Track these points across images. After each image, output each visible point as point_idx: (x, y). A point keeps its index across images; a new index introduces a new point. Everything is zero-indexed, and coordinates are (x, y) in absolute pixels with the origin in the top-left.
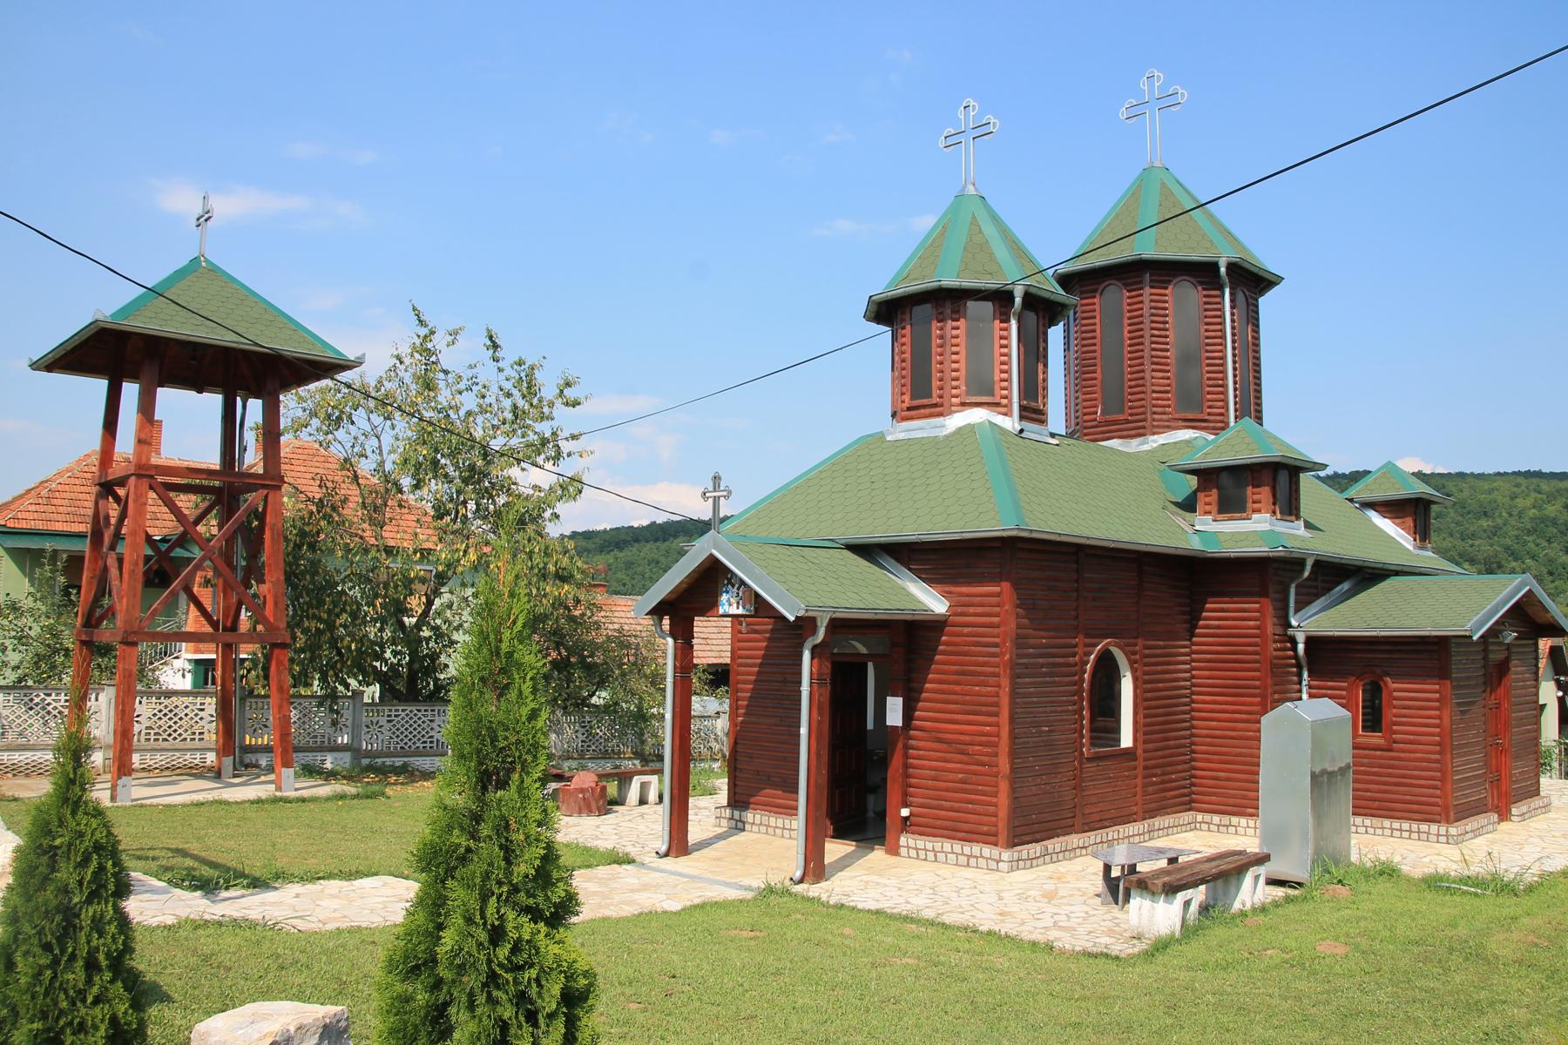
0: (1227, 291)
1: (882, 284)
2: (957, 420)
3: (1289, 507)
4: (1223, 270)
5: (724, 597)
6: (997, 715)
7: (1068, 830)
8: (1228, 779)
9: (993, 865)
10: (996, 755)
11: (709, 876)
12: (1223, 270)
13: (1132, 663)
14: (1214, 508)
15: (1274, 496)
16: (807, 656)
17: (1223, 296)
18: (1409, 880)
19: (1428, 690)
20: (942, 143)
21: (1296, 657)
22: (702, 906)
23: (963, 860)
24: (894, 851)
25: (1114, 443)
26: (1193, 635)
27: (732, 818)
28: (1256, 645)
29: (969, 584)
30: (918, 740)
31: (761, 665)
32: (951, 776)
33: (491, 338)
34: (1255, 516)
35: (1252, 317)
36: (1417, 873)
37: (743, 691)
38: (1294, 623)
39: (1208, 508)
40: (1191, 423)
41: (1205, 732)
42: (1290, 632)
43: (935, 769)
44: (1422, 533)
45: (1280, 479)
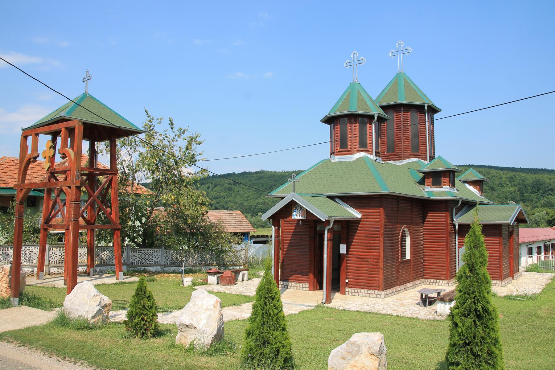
0: (427, 114)
3: (453, 184)
4: (426, 108)
5: (294, 213)
10: (379, 262)
12: (426, 108)
13: (410, 232)
16: (326, 232)
18: (500, 297)
21: (455, 230)
22: (303, 311)
24: (344, 293)
25: (391, 162)
26: (424, 224)
27: (283, 285)
29: (369, 209)
30: (351, 258)
31: (292, 235)
32: (363, 269)
33: (171, 121)
34: (444, 187)
35: (432, 121)
38: (455, 220)
42: (454, 222)
44: (481, 191)
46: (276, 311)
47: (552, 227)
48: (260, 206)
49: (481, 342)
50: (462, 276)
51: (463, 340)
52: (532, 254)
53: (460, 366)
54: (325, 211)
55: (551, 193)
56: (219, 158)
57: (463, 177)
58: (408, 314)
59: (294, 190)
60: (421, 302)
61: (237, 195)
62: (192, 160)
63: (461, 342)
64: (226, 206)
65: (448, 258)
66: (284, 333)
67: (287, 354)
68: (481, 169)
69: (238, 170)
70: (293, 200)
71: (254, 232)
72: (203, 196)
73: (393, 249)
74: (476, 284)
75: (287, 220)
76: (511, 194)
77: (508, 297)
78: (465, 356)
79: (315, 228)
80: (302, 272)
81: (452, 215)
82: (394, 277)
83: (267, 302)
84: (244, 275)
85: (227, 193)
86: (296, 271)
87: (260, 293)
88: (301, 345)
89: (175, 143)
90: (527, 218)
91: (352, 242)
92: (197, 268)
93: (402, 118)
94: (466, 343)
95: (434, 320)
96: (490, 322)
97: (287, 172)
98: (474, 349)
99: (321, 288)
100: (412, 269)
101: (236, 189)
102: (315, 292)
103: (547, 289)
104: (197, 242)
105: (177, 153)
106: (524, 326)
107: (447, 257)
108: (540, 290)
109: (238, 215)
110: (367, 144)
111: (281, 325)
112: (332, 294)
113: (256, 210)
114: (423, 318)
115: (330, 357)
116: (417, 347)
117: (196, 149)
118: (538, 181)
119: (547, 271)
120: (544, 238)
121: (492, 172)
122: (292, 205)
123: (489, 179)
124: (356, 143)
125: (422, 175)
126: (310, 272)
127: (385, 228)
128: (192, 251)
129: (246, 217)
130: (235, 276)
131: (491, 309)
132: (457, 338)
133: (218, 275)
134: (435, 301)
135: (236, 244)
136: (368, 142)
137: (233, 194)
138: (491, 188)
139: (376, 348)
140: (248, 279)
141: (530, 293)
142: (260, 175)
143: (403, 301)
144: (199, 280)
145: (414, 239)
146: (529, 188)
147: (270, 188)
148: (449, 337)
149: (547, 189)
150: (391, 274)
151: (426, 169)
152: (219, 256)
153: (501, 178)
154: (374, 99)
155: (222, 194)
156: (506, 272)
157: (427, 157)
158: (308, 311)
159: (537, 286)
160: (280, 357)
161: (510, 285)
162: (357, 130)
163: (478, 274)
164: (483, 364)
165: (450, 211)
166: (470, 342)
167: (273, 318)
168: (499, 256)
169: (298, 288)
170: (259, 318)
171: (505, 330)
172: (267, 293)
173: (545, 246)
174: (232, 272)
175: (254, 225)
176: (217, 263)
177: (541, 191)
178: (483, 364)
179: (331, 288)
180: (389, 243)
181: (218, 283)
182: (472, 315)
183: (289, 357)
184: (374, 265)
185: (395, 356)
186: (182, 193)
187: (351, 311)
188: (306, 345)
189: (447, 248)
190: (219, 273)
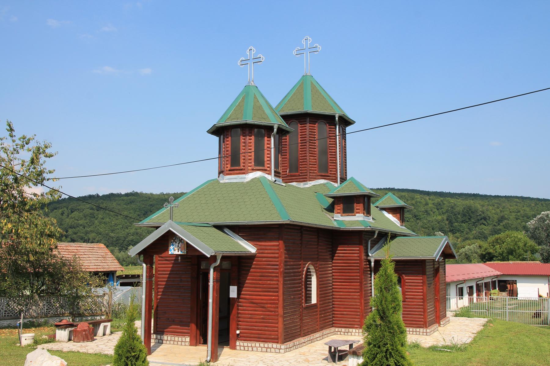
0: (338, 127)
3: (368, 212)
4: (337, 118)
5: (172, 247)
8: (347, 314)
9: (277, 351)
10: (277, 307)
11: (168, 362)
12: (337, 118)
13: (316, 271)
17: (336, 128)
18: (424, 349)
20: (239, 63)
21: (370, 267)
24: (234, 348)
25: (294, 184)
26: (333, 260)
27: (157, 339)
29: (265, 241)
31: (169, 274)
32: (258, 317)
33: (10, 126)
34: (357, 215)
35: (344, 135)
37: (161, 285)
38: (370, 255)
39: (339, 211)
42: (369, 258)
44: (402, 220)
45: (361, 201)
47: (485, 262)
48: (131, 237)
50: (371, 325)
52: (462, 295)
54: (210, 245)
55: (485, 222)
56: (76, 175)
57: (381, 203)
59: (171, 218)
60: (329, 357)
61: (100, 223)
62: (39, 178)
64: (86, 238)
65: (363, 301)
68: (403, 194)
69: (103, 191)
70: (170, 230)
71: (121, 270)
72: (52, 224)
73: (295, 291)
75: (162, 255)
76: (439, 223)
77: (433, 349)
79: (199, 265)
84: (105, 327)
85: (88, 221)
86: (174, 321)
89: (16, 155)
90: (455, 253)
92: (43, 320)
99: (205, 342)
100: (318, 316)
101: (100, 216)
102: (197, 347)
103: (480, 337)
104: (43, 285)
105: (17, 168)
107: (361, 301)
109: (100, 249)
110: (264, 161)
112: (219, 350)
113: (125, 243)
117: (46, 164)
118: (470, 208)
119: (480, 315)
120: (476, 276)
121: (416, 197)
123: (413, 205)
124: (250, 159)
125: (331, 200)
126: (191, 322)
127: (285, 265)
128: (37, 297)
129: (112, 252)
130: (93, 329)
133: (70, 329)
134: (346, 355)
135: (96, 286)
136: (266, 159)
137: (96, 222)
138: (415, 216)
140: (112, 333)
141: (460, 342)
142: (132, 198)
144: (44, 337)
145: (320, 278)
146: (459, 216)
147: (144, 214)
149: (479, 218)
150: (293, 322)
151: (335, 193)
152: (73, 304)
153: (427, 204)
154: (274, 106)
155: (81, 222)
157: (337, 178)
161: (436, 334)
162: (253, 144)
168: (422, 299)
172: (129, 351)
173: (477, 285)
174: (90, 324)
175: (122, 262)
176: (70, 313)
180: (290, 284)
181: (70, 340)
184: (271, 311)
186: (23, 220)
189: (361, 289)
190: (71, 325)
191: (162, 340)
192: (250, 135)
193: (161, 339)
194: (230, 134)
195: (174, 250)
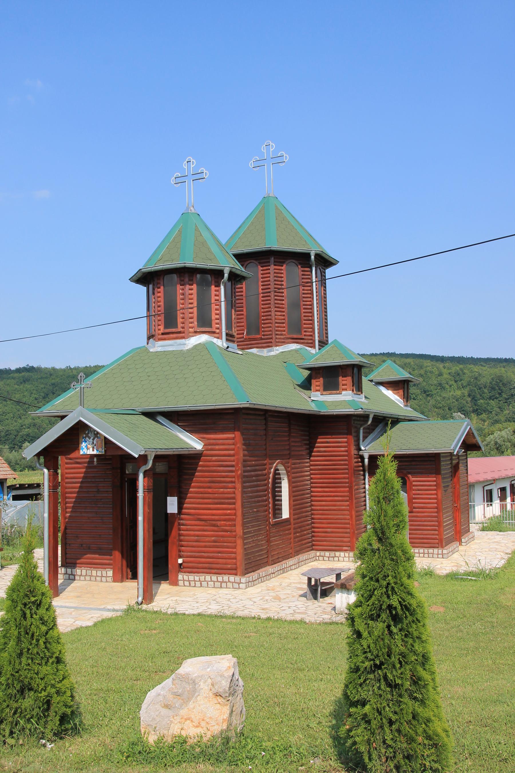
0: (314, 269)
1: (141, 263)
2: (194, 341)
3: (358, 388)
4: (313, 257)
5: (84, 445)
6: (234, 504)
7: (267, 564)
8: (332, 532)
9: (236, 586)
10: (235, 525)
11: (83, 606)
12: (313, 257)
13: (288, 472)
14: (322, 388)
15: (353, 382)
17: (311, 272)
18: (440, 577)
19: (430, 480)
20: (173, 181)
21: (363, 466)
22: (103, 621)
23: (218, 584)
24: (175, 583)
25: (254, 351)
26: (311, 456)
27: (66, 573)
28: (345, 460)
29: (215, 433)
31: (82, 482)
32: (208, 539)
34: (344, 392)
36: (444, 572)
38: (363, 448)
39: (318, 388)
40: (296, 340)
41: (319, 508)
42: (361, 453)
43: (198, 536)
44: (407, 398)
45: (351, 373)
46: (44, 628)
48: (26, 431)
49: (400, 663)
50: (365, 550)
51: (371, 660)
52: (491, 501)
53: (367, 707)
54: (139, 440)
57: (375, 375)
58: (287, 614)
59: (82, 404)
60: (309, 592)
63: (367, 664)
65: (353, 513)
66: (60, 667)
67: (66, 706)
70: (80, 422)
73: (258, 502)
74: (389, 562)
75: (72, 455)
76: (457, 400)
78: (375, 688)
79: (123, 469)
80: (100, 549)
81: (358, 440)
82: (261, 550)
83: (28, 612)
86: (89, 548)
87: (15, 597)
88: (95, 686)
90: (480, 443)
91: (187, 492)
93: (272, 276)
94: (375, 665)
95: (331, 624)
96: (414, 626)
97: (75, 369)
98: (389, 675)
99: (135, 576)
100: (292, 536)
102: (124, 584)
106: (478, 625)
108: (503, 562)
110: (211, 320)
111: (53, 653)
112: (154, 586)
113: (18, 438)
114: (313, 620)
115: (144, 706)
116: (301, 675)
118: (500, 379)
121: (425, 364)
122: (79, 430)
123: (421, 376)
124: (191, 318)
125: (307, 373)
126: (114, 549)
127: (244, 466)
131: (414, 605)
132: (361, 658)
134: (332, 589)
136: (214, 317)
138: (425, 392)
139: (225, 684)
143: (278, 594)
146: (486, 391)
147: (44, 398)
148: (348, 656)
153: (441, 374)
154: (223, 241)
156: (448, 533)
157: (314, 341)
158: (110, 619)
159: (500, 555)
160: (52, 713)
162: (195, 296)
163: (391, 545)
164: (405, 699)
165: (354, 434)
166: (382, 663)
167: (38, 640)
168: (437, 508)
169: (93, 578)
170: (12, 643)
171: (447, 633)
172: (27, 595)
175: (14, 466)
177: (504, 396)
178: (405, 699)
179: (151, 575)
180: (252, 492)
182: (384, 616)
183: (69, 711)
184: (227, 531)
185: (262, 693)
187: (189, 615)
188: (104, 686)
191: (74, 576)
192: (190, 282)
193: (72, 574)
194: (162, 283)
195: (88, 449)
